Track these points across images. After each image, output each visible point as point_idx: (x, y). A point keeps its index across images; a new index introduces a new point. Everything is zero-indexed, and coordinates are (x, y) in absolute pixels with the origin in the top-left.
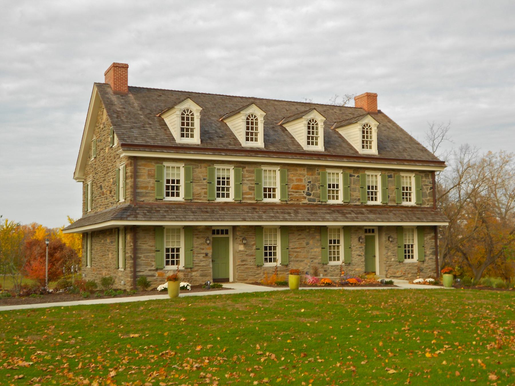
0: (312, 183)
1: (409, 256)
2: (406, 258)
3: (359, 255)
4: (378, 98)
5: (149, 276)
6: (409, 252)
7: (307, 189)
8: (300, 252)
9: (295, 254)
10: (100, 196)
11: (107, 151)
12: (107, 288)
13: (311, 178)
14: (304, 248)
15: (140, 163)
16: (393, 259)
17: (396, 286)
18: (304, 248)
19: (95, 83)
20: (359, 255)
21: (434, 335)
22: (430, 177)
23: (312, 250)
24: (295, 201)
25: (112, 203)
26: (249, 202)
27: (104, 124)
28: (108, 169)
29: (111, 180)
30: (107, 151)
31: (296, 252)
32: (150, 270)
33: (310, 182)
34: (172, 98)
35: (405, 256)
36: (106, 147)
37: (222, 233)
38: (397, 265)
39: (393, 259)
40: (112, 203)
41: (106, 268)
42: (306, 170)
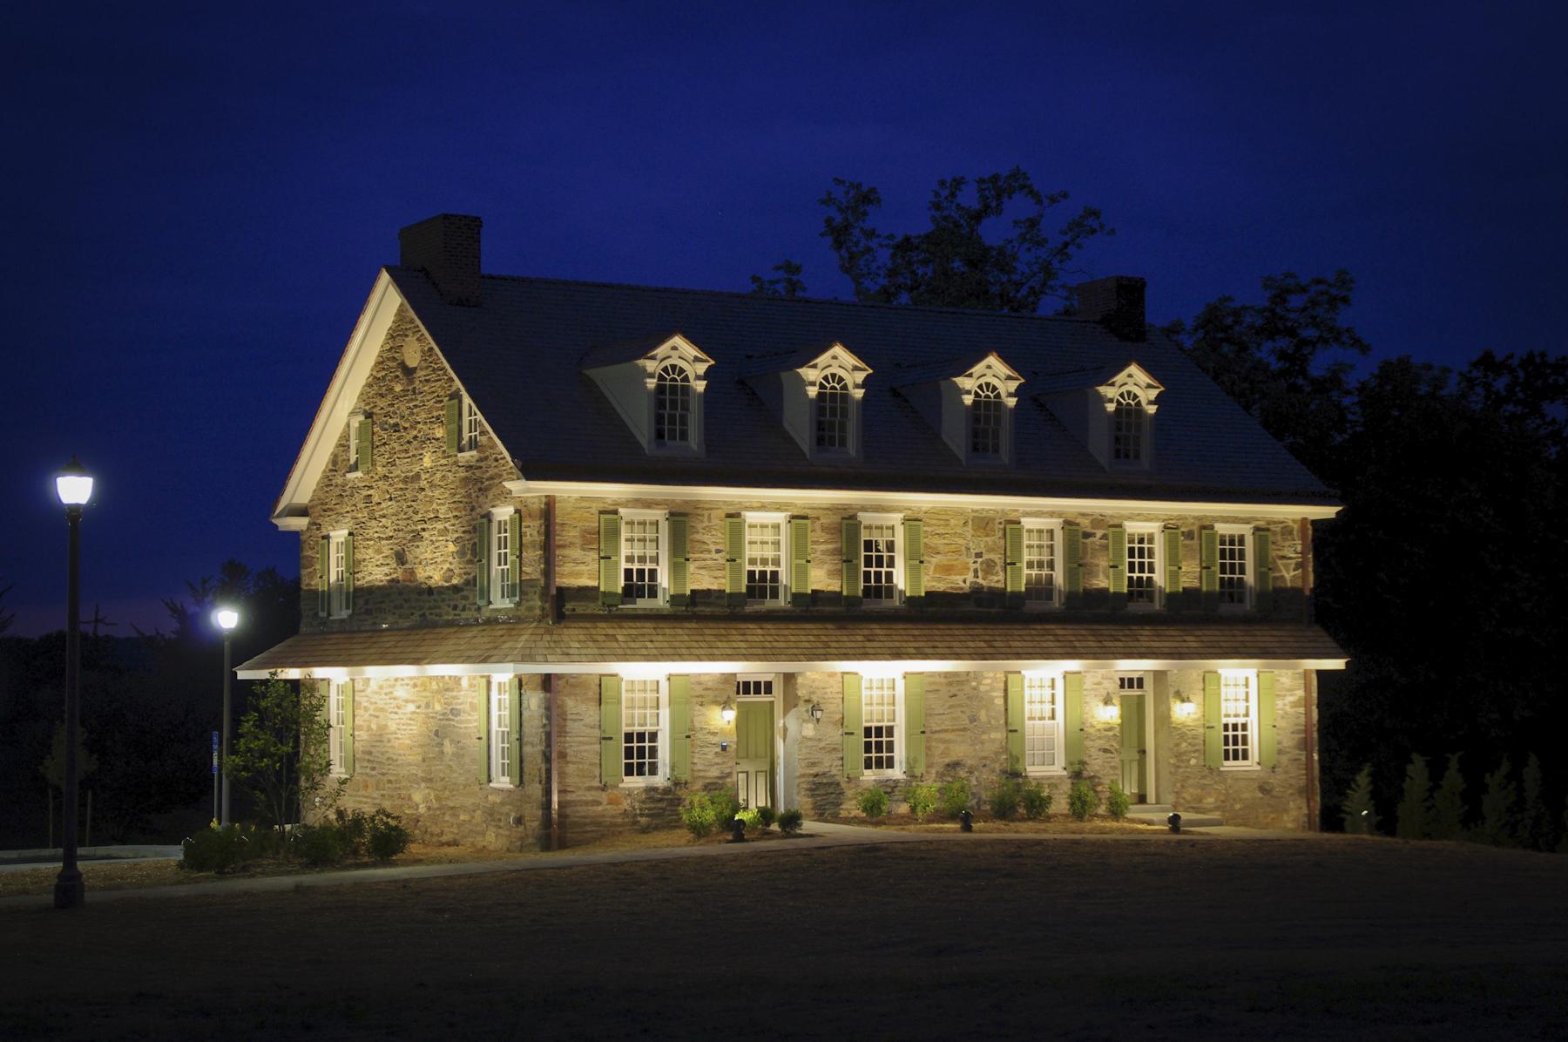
0: (986, 556)
1: (641, 766)
2: (1227, 758)
3: (1105, 751)
4: (1148, 292)
5: (586, 803)
6: (1235, 743)
9: (942, 747)
14: (964, 729)
16: (1193, 762)
17: (1185, 833)
18: (964, 729)
20: (1105, 751)
23: (985, 737)
26: (828, 609)
31: (945, 741)
32: (590, 789)
33: (979, 555)
34: (992, 248)
35: (1227, 751)
37: (757, 692)
38: (1203, 777)
39: (1193, 762)
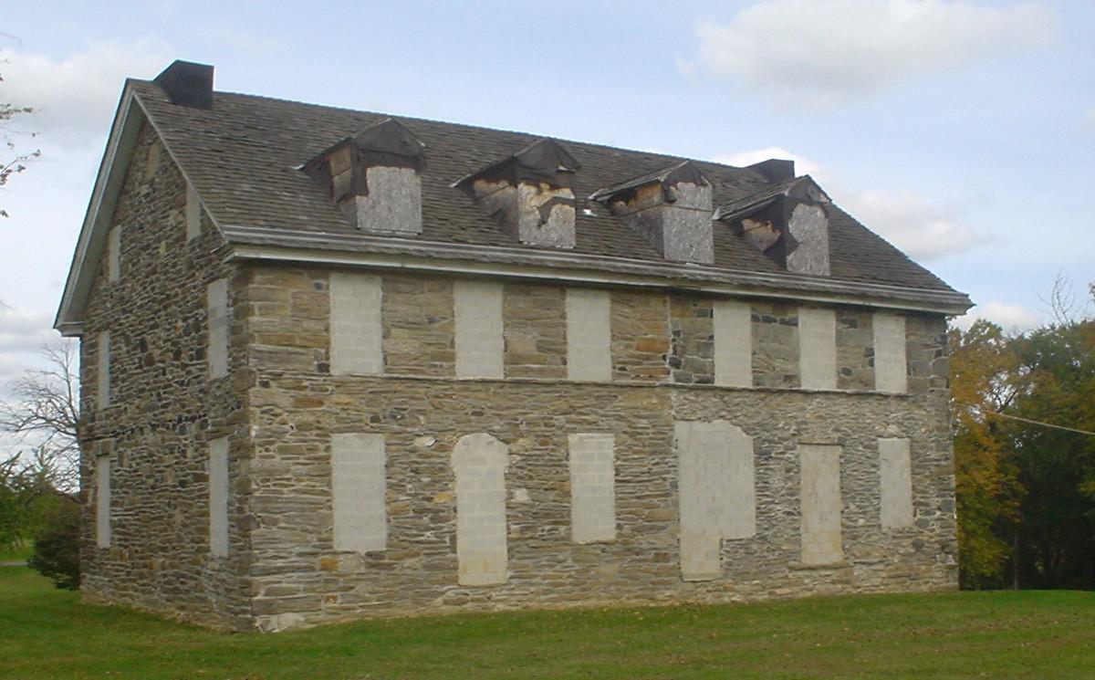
7: (671, 351)
8: (658, 507)
10: (141, 367)
11: (162, 251)
12: (941, 386)
13: (685, 323)
15: (259, 282)
19: (128, 81)
21: (1020, 386)
22: (769, 226)
24: (644, 379)
25: (182, 384)
27: (152, 183)
28: (168, 297)
29: (180, 323)
30: (162, 251)
36: (159, 240)
40: (182, 384)
41: (164, 549)
42: (669, 303)
